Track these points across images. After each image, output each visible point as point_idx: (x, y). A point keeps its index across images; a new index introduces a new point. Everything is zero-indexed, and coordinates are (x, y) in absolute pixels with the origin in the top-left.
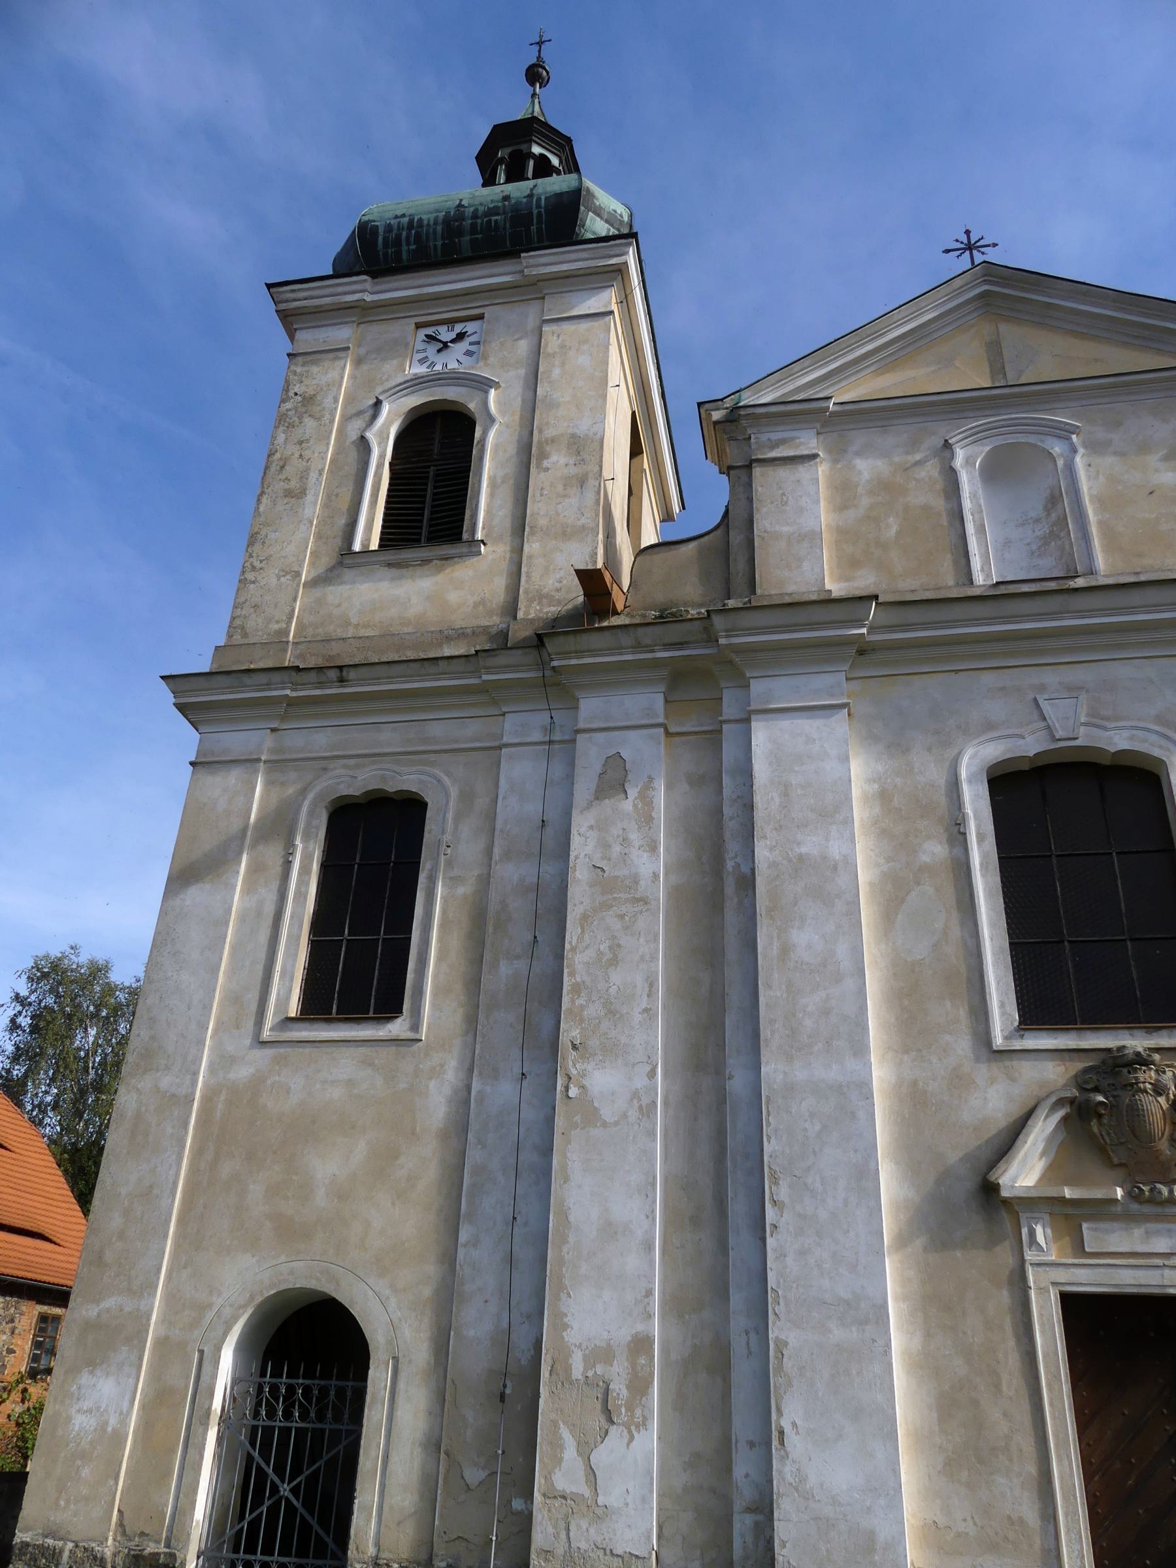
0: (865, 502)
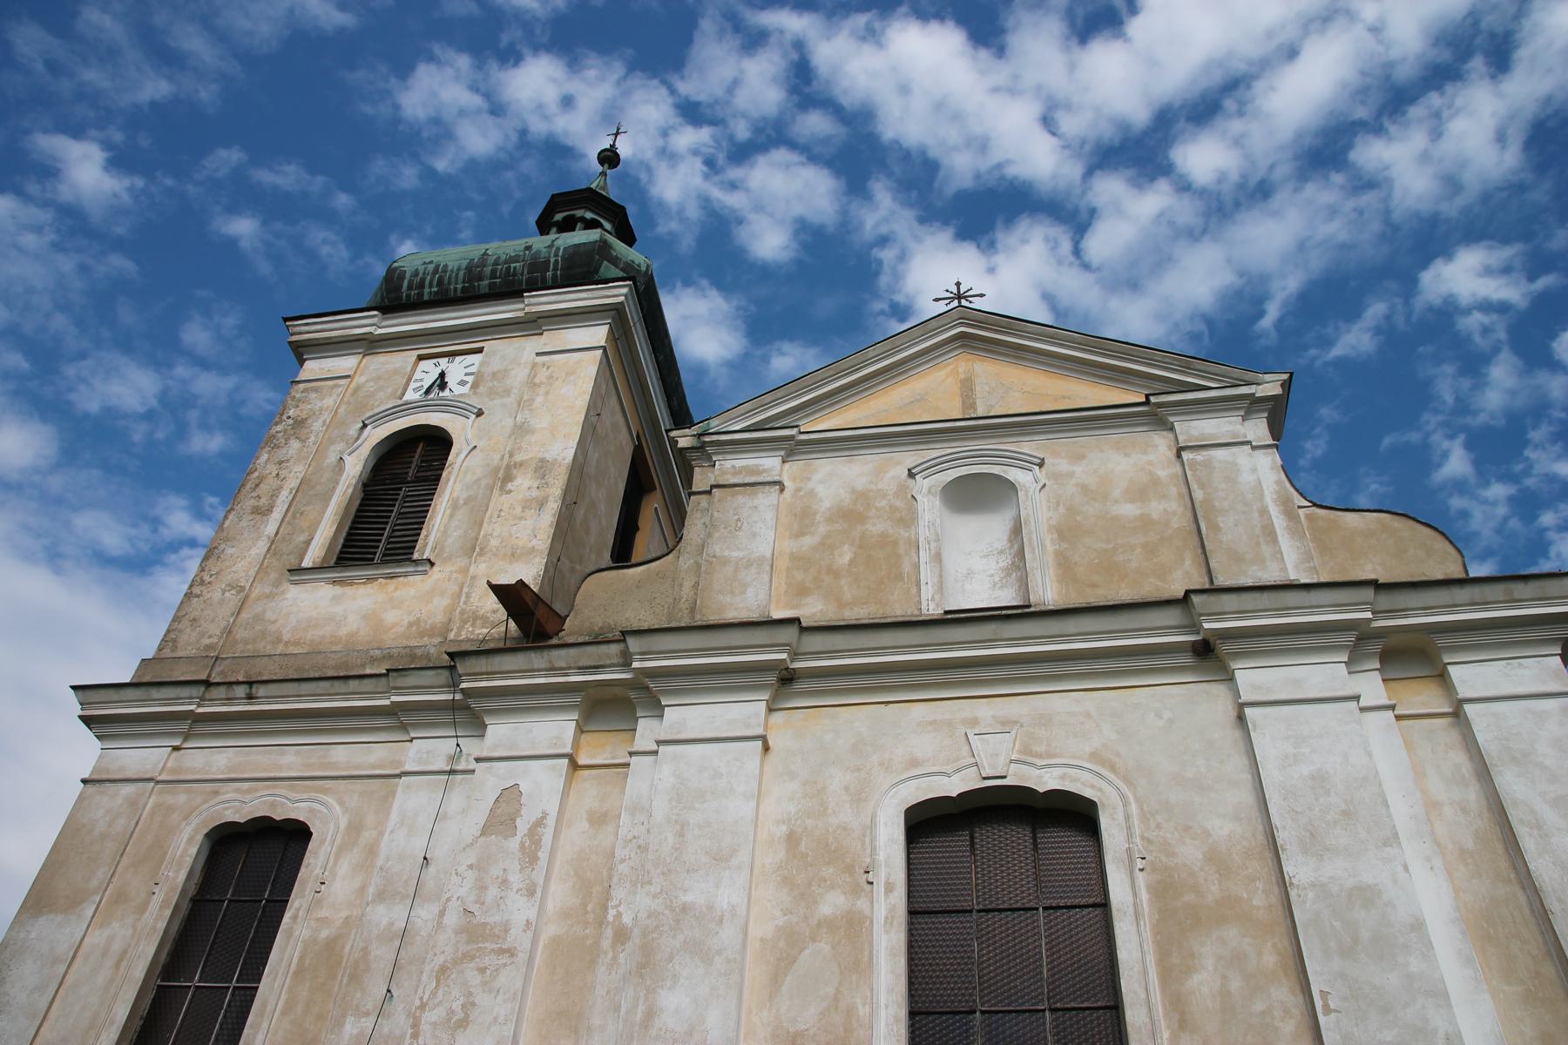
0: (822, 529)
